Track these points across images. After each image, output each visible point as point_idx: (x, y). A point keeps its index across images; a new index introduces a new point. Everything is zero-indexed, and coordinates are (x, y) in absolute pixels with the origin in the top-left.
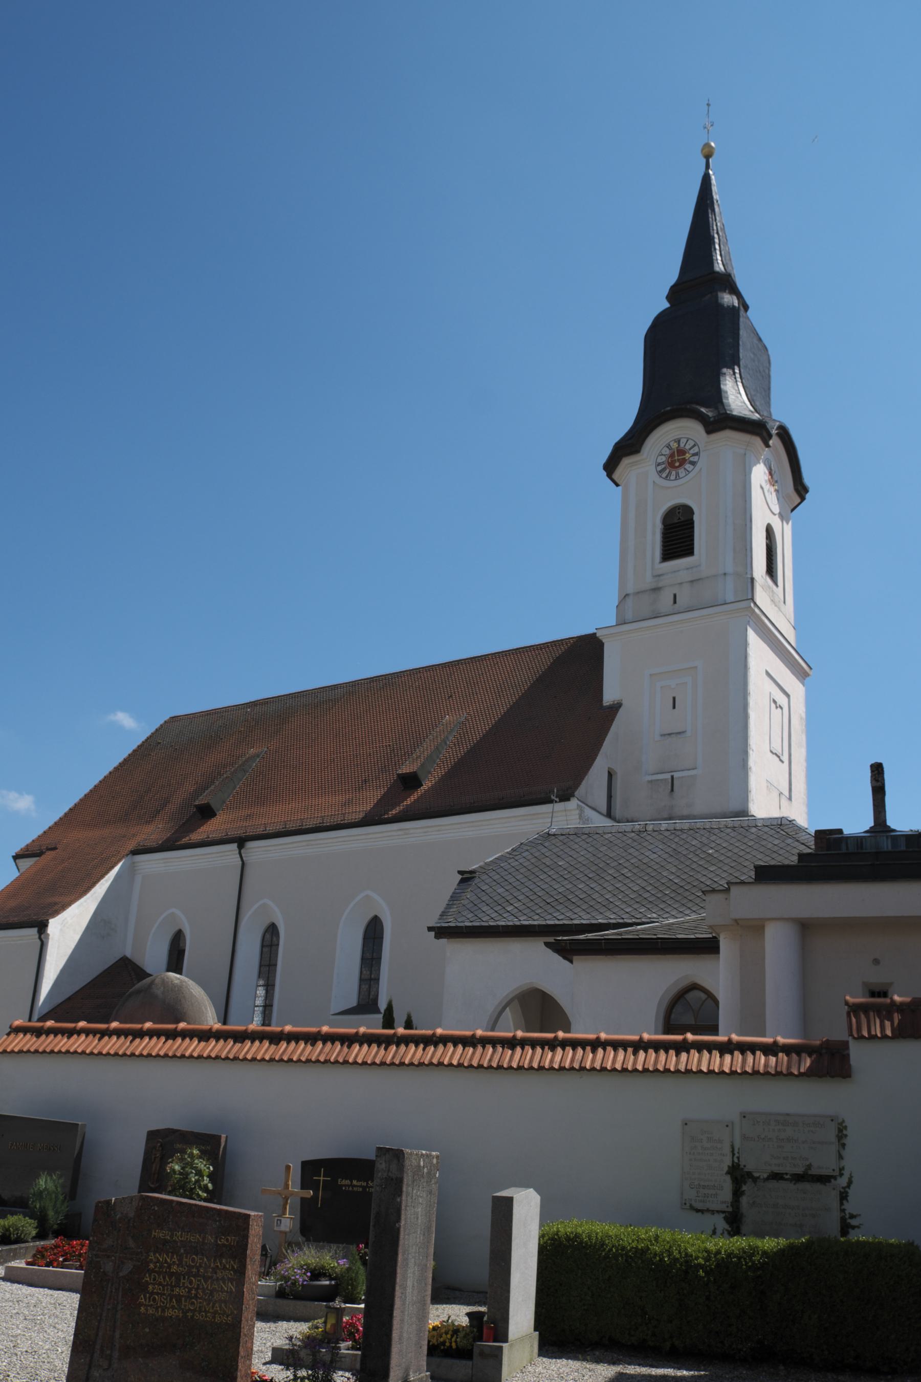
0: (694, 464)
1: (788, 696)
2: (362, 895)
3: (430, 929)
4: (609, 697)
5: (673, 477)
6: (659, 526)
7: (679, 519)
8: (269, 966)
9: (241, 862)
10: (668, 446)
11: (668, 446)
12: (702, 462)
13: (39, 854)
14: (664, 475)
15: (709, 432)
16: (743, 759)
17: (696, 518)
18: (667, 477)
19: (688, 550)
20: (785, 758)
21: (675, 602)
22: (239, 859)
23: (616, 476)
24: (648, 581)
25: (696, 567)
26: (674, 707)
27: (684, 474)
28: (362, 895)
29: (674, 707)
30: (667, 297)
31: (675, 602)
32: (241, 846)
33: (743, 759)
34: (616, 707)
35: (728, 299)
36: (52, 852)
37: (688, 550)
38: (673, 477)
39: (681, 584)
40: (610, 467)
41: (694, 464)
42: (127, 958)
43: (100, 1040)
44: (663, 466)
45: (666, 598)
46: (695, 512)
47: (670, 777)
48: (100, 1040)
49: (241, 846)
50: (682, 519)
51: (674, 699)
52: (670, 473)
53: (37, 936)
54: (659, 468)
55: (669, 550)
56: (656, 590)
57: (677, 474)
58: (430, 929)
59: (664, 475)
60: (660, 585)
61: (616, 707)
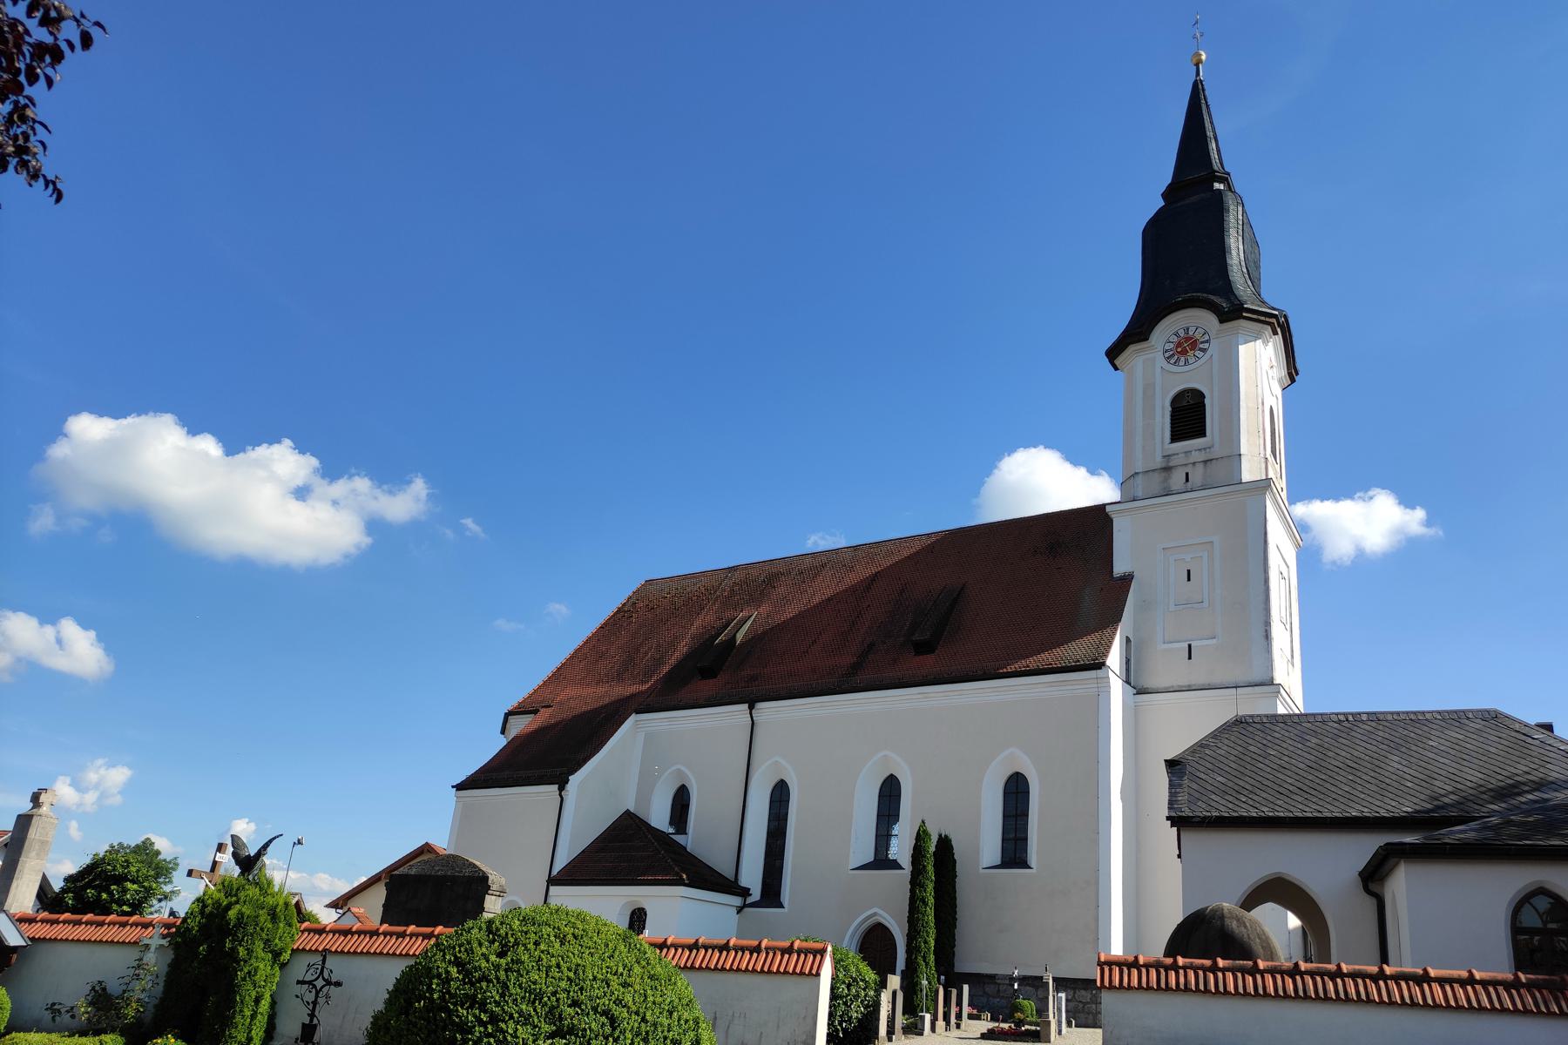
0: (1204, 350)
1: (1288, 567)
2: (882, 754)
3: (453, 787)
4: (1119, 568)
5: (1182, 363)
6: (1169, 409)
7: (1188, 402)
8: (1016, 816)
9: (750, 722)
10: (1176, 334)
11: (1176, 334)
12: (1213, 348)
13: (535, 712)
14: (1173, 361)
15: (1221, 322)
16: (1266, 631)
17: (1207, 401)
18: (1175, 363)
19: (1201, 432)
20: (1288, 627)
21: (1187, 480)
22: (750, 719)
23: (1117, 362)
24: (1158, 462)
25: (1210, 448)
26: (1189, 579)
27: (1193, 360)
28: (882, 754)
29: (1189, 579)
30: (1162, 195)
31: (1187, 480)
32: (751, 708)
33: (1266, 631)
34: (1127, 579)
35: (1218, 186)
36: (547, 709)
37: (1201, 432)
38: (1182, 363)
39: (1194, 464)
40: (1113, 353)
41: (1204, 350)
42: (631, 813)
43: (73, 926)
44: (1171, 353)
45: (1177, 479)
46: (1202, 390)
47: (1187, 646)
48: (73, 926)
49: (751, 708)
50: (1192, 402)
51: (1189, 571)
52: (1173, 355)
53: (558, 793)
54: (1167, 355)
55: (1177, 431)
56: (1167, 469)
57: (1186, 361)
58: (453, 787)
59: (1173, 361)
60: (1171, 464)
61: (1127, 579)
